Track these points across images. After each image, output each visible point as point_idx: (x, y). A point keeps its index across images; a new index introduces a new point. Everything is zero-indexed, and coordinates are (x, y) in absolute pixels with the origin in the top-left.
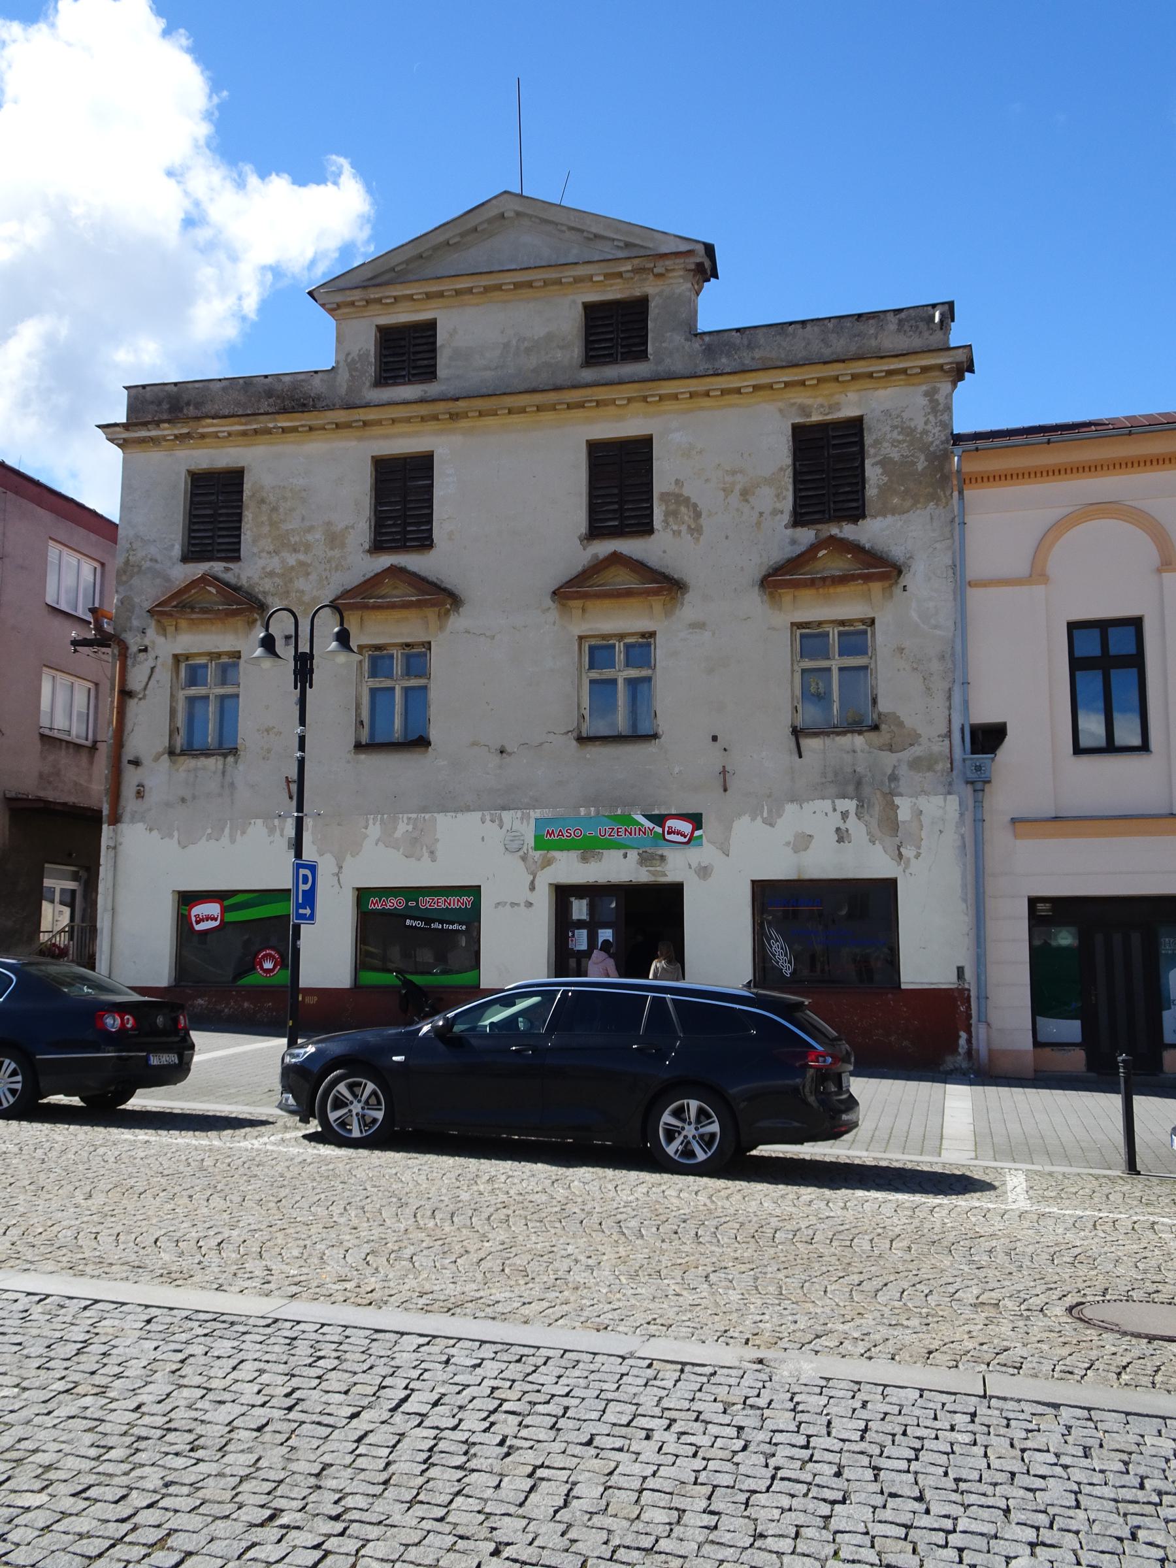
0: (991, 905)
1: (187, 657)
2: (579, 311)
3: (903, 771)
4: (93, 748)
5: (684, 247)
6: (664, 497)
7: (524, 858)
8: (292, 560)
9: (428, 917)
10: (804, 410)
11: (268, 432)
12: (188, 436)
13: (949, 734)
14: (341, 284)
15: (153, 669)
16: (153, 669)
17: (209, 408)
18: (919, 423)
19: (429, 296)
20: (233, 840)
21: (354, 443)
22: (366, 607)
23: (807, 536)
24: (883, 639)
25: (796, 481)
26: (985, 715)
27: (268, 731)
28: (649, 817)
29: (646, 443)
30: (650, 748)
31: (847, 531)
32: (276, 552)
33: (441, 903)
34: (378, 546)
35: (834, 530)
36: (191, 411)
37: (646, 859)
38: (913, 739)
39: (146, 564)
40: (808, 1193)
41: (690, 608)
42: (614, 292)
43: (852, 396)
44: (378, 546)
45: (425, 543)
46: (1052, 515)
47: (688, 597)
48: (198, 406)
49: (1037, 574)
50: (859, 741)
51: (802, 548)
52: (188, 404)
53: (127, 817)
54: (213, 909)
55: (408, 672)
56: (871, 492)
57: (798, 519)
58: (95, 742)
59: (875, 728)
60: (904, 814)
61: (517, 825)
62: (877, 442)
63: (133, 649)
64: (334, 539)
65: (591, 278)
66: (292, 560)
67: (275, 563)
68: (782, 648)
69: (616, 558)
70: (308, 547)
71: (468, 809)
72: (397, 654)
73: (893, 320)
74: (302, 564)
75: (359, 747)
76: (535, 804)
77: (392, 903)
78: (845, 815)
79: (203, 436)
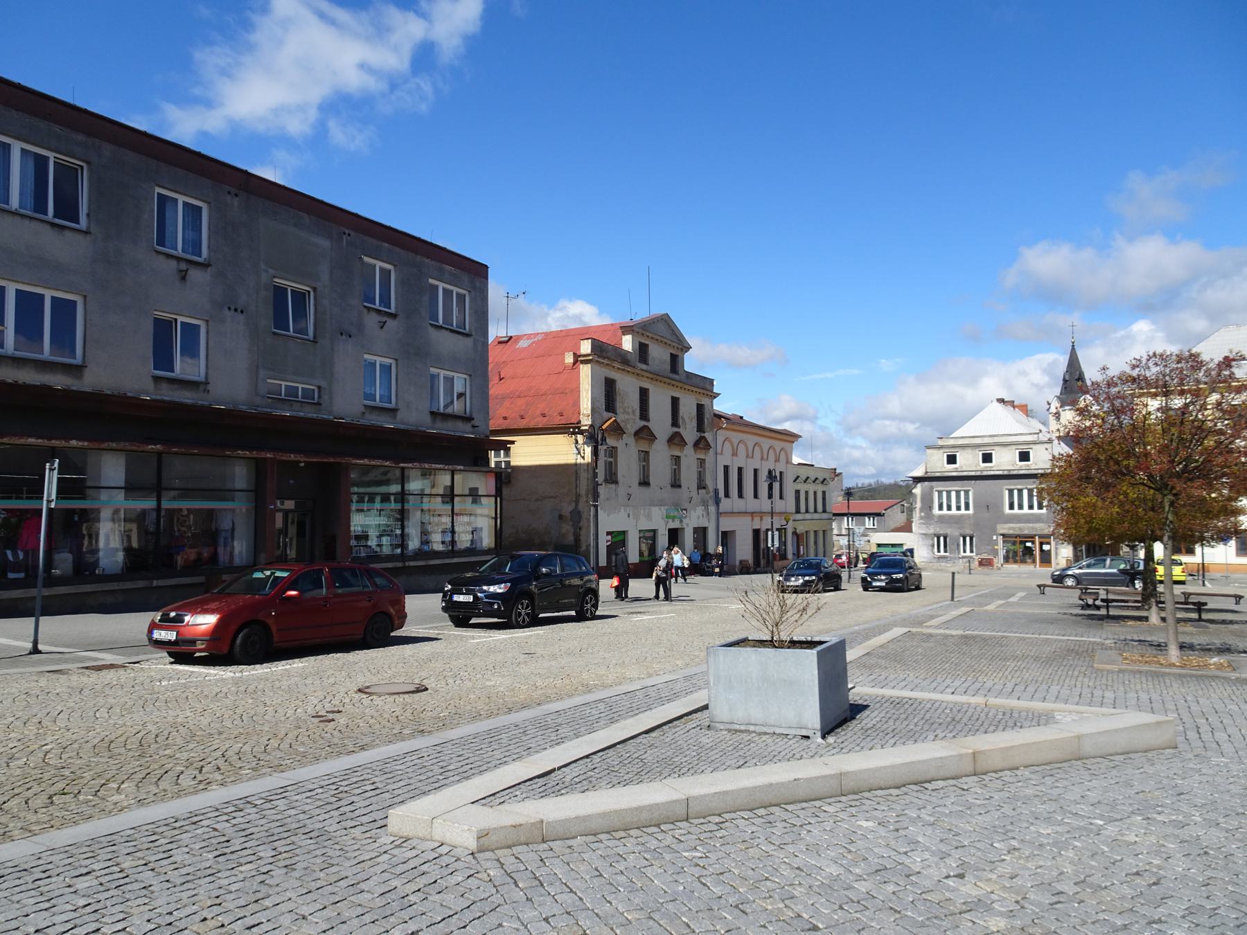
30: (678, 490)
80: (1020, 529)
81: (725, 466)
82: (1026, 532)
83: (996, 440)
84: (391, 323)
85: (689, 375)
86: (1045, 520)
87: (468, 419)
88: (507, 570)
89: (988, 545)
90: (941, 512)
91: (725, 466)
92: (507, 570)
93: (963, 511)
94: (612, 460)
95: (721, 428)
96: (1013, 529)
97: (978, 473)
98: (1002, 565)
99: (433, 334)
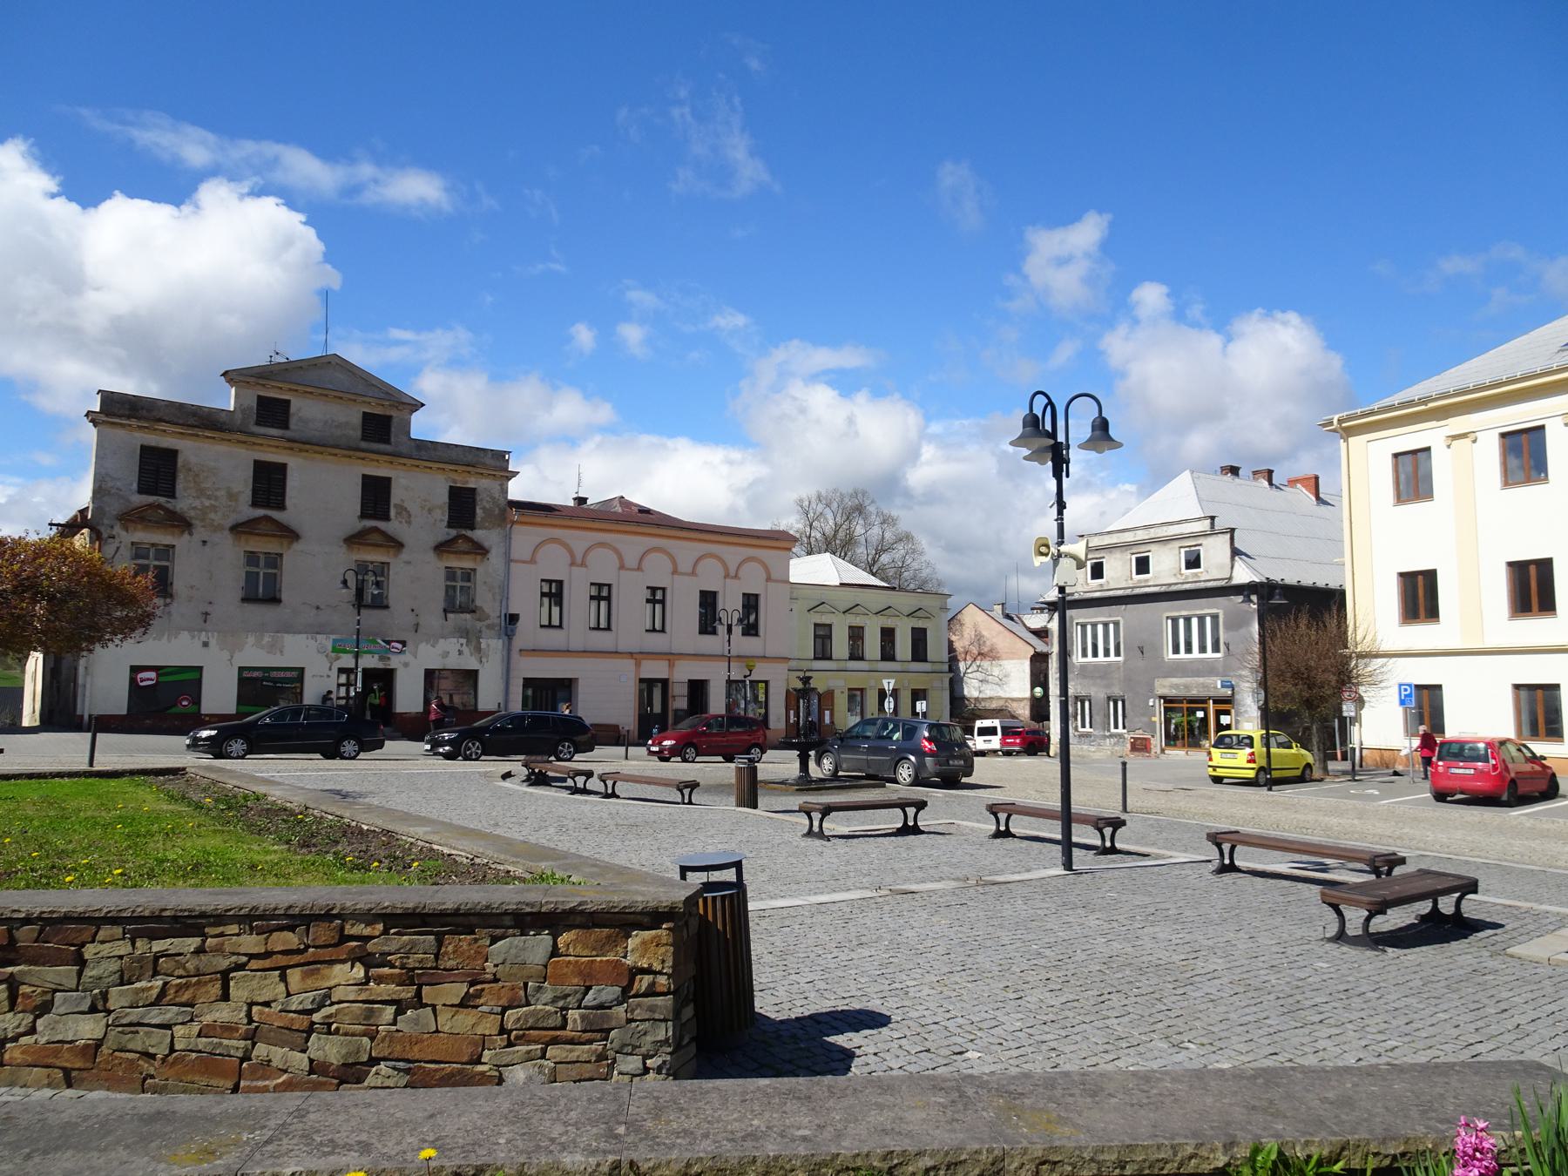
0: (511, 681)
1: (138, 543)
2: (360, 416)
3: (484, 629)
5: (414, 402)
6: (395, 505)
7: (327, 656)
8: (207, 503)
9: (275, 681)
10: (455, 481)
11: (197, 436)
13: (500, 617)
14: (244, 372)
15: (118, 548)
16: (118, 548)
18: (497, 496)
19: (290, 390)
20: (169, 641)
21: (244, 451)
22: (251, 533)
23: (453, 532)
24: (480, 576)
25: (450, 509)
26: (512, 611)
27: (192, 587)
28: (384, 641)
29: (389, 480)
30: (385, 612)
31: (469, 533)
32: (198, 498)
33: (282, 674)
34: (255, 504)
35: (464, 532)
37: (382, 659)
38: (488, 617)
39: (113, 491)
40: (150, 766)
41: (405, 555)
42: (378, 411)
43: (473, 479)
44: (255, 504)
45: (281, 506)
46: (539, 540)
47: (404, 550)
48: (149, 411)
49: (533, 561)
50: (468, 616)
51: (450, 537)
52: (142, 408)
54: (153, 675)
55: (454, 588)
56: (478, 519)
57: (450, 525)
59: (474, 612)
60: (483, 646)
61: (324, 641)
62: (481, 500)
64: (232, 496)
65: (369, 403)
66: (207, 503)
67: (197, 503)
68: (442, 574)
69: (376, 530)
70: (216, 498)
71: (300, 633)
72: (262, 556)
73: (490, 454)
74: (212, 506)
75: (245, 600)
76: (332, 633)
77: (255, 674)
78: (462, 645)
79: (156, 430)
80: (1187, 687)
81: (704, 594)
82: (1194, 693)
83: (1153, 533)
85: (422, 445)
86: (1221, 670)
89: (1143, 715)
90: (1085, 660)
91: (704, 594)
93: (1112, 658)
95: (513, 523)
96: (1176, 686)
97: (1128, 592)
98: (1163, 751)
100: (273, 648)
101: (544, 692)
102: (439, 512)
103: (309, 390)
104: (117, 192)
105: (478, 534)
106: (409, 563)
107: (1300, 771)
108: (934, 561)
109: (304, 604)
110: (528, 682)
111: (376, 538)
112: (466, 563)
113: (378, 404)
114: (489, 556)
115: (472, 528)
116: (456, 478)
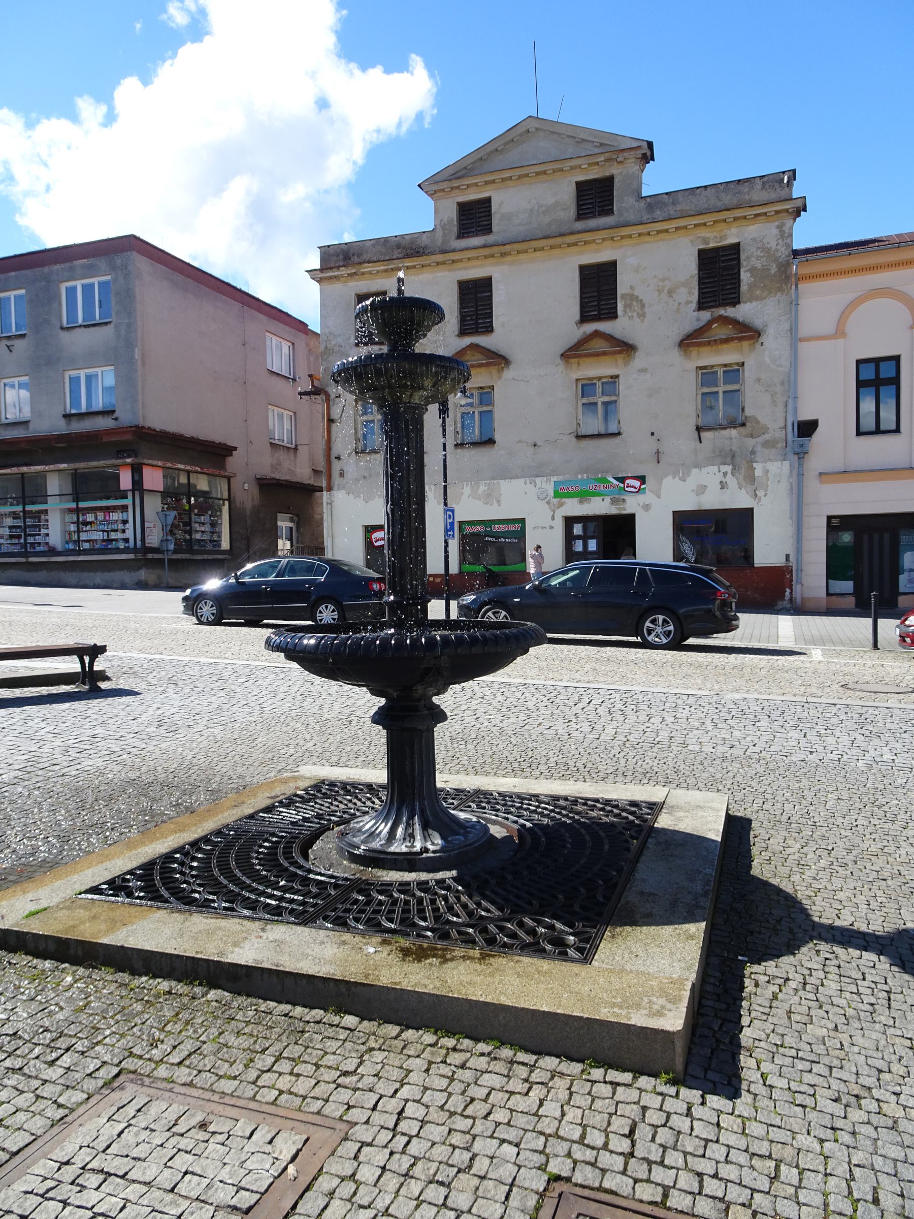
3: (759, 448)
4: (296, 449)
5: (635, 144)
7: (548, 503)
9: (497, 535)
10: (705, 240)
12: (355, 274)
13: (785, 427)
14: (436, 179)
17: (365, 257)
18: (773, 245)
19: (487, 183)
21: (446, 273)
23: (706, 315)
24: (748, 373)
26: (806, 415)
28: (616, 479)
31: (730, 312)
33: (503, 528)
36: (356, 259)
37: (614, 501)
38: (765, 430)
41: (639, 361)
45: (489, 329)
46: (852, 296)
49: (840, 333)
50: (734, 432)
52: (354, 255)
53: (335, 487)
56: (744, 288)
57: (701, 306)
58: (296, 446)
59: (743, 425)
60: (758, 472)
62: (748, 258)
63: (333, 396)
71: (517, 477)
77: (478, 529)
78: (725, 474)
79: (363, 274)
84: (18, 344)
87: (108, 413)
88: (682, 611)
92: (682, 611)
94: (599, 384)
99: (65, 336)
100: (490, 497)
101: (876, 537)
102: (683, 291)
103: (506, 175)
104: (418, 63)
105: (744, 311)
106: (644, 371)
107: (284, 342)
108: (450, 964)
109: (520, 441)
110: (836, 524)
111: (599, 345)
112: (728, 356)
113: (590, 165)
114: (763, 339)
115: (735, 301)
116: (709, 235)
